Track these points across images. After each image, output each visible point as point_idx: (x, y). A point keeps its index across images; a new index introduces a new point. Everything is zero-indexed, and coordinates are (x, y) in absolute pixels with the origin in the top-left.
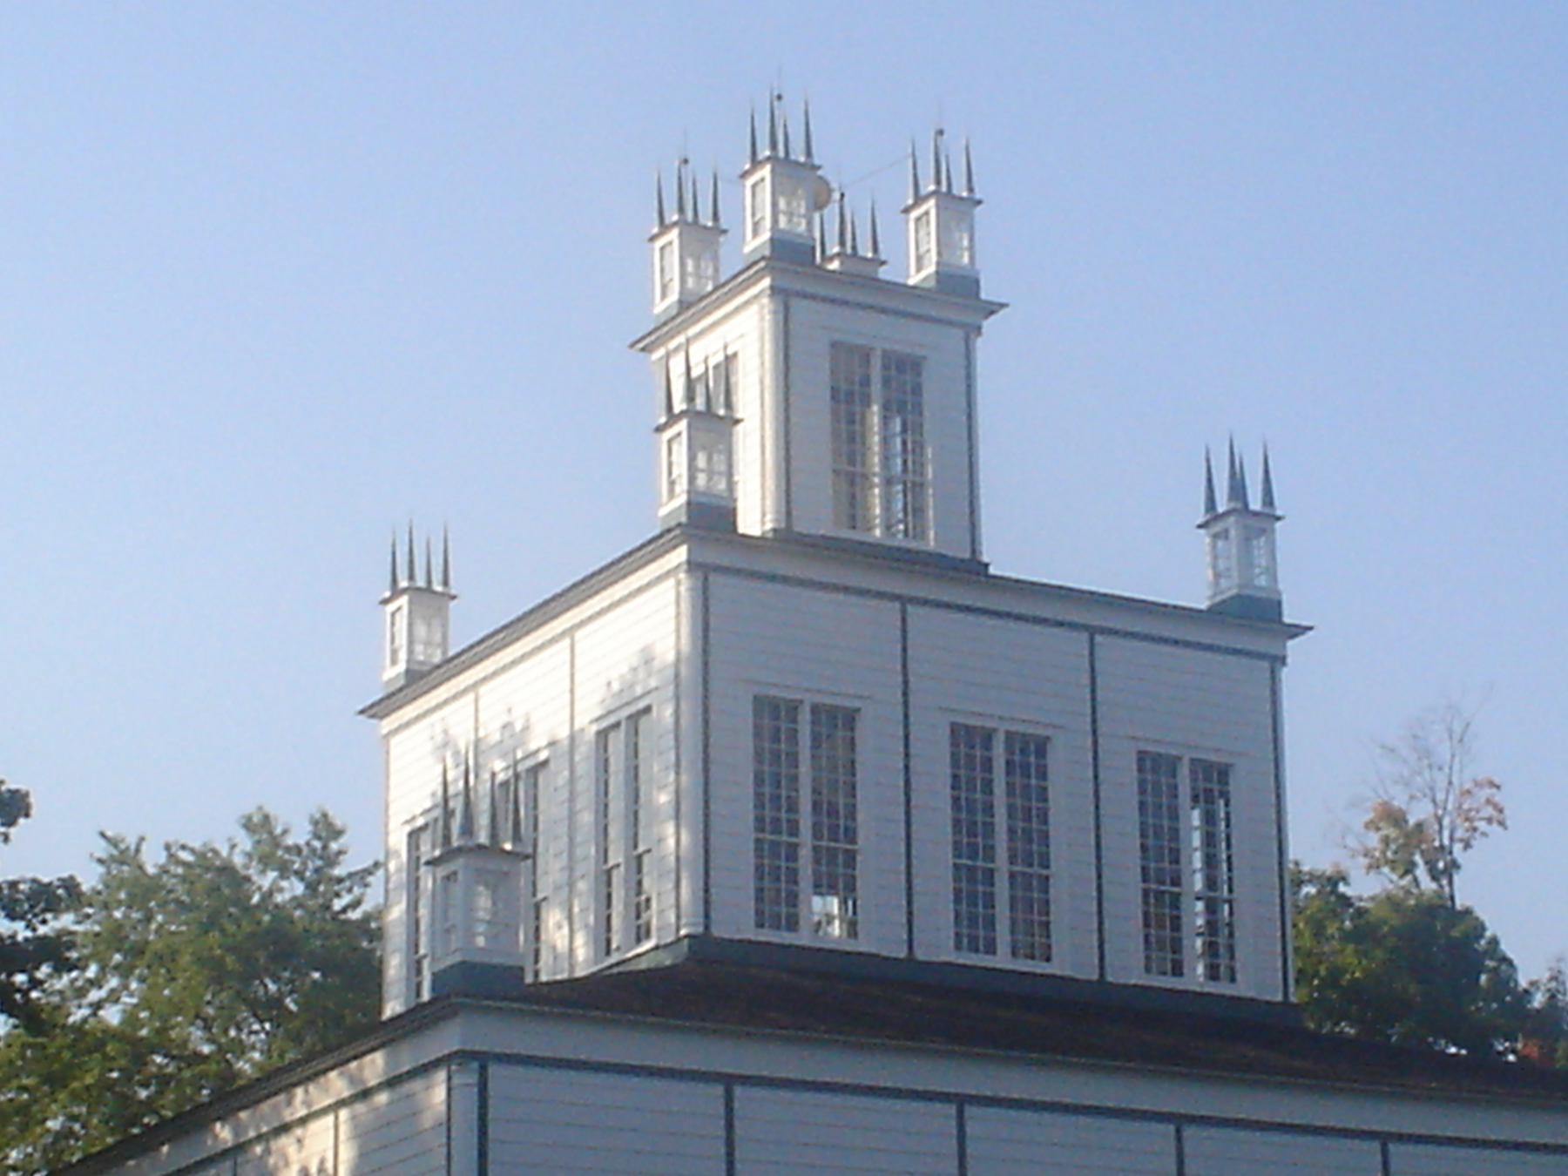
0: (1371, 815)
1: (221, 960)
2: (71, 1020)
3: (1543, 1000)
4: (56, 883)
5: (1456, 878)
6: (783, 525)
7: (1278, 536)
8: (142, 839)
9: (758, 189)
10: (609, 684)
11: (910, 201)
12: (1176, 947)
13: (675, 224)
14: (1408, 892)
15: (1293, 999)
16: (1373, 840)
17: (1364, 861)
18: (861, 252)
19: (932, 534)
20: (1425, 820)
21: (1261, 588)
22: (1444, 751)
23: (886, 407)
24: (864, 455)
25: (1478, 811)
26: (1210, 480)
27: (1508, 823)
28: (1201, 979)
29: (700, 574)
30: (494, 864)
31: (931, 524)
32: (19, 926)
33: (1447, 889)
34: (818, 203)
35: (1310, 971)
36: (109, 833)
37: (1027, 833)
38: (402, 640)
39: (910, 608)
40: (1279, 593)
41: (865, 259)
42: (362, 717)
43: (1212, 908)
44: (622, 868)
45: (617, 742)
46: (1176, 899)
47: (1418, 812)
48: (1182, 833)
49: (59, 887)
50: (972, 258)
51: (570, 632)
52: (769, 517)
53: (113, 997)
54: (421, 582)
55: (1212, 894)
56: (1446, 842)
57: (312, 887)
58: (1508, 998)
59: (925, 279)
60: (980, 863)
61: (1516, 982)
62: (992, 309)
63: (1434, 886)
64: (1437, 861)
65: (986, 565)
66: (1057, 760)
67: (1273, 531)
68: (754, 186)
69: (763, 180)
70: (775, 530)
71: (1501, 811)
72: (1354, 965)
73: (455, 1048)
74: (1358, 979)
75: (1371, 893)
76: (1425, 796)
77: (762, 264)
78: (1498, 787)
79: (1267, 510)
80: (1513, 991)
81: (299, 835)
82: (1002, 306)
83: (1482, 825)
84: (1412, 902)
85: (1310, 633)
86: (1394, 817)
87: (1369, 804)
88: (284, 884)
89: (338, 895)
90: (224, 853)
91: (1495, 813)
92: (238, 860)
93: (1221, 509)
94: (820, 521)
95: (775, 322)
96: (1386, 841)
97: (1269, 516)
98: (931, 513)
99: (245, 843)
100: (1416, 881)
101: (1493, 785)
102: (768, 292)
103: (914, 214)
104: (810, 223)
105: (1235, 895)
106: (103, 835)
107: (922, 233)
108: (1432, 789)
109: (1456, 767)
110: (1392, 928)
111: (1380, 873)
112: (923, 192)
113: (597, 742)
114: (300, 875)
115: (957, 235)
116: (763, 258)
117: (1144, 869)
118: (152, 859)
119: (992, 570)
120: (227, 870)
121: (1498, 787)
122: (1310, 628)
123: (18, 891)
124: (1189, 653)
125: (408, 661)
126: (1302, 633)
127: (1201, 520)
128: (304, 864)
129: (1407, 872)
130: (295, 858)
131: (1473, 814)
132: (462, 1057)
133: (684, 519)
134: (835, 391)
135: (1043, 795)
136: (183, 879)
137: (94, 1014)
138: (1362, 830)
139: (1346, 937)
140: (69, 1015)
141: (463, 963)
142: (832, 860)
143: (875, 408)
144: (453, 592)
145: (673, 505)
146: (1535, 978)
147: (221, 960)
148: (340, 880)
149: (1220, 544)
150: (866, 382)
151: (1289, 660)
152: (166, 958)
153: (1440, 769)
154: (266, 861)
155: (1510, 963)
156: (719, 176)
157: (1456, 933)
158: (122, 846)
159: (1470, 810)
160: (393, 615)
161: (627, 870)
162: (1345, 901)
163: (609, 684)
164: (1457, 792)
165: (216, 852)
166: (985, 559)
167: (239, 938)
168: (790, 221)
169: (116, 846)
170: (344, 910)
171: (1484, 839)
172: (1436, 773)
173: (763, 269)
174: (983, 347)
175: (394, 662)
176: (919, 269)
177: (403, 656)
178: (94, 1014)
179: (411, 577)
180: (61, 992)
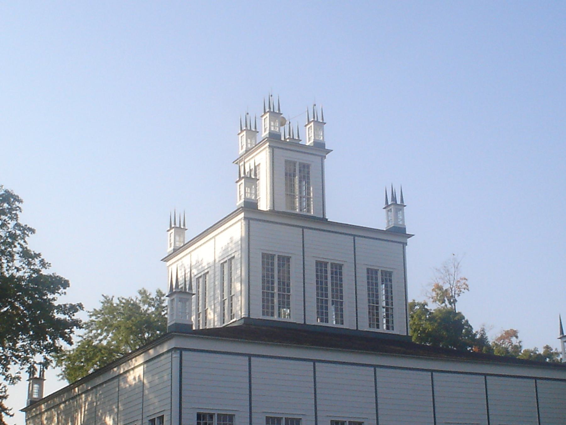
0: (434, 287)
1: (131, 328)
2: (94, 344)
3: (480, 336)
4: (77, 305)
5: (456, 304)
6: (272, 209)
7: (405, 211)
8: (113, 297)
9: (266, 120)
10: (222, 248)
11: (307, 123)
12: (378, 320)
13: (245, 130)
14: (444, 308)
15: (409, 335)
16: (434, 294)
17: (432, 300)
18: (295, 138)
19: (312, 211)
20: (448, 289)
21: (400, 225)
22: (452, 271)
23: (300, 178)
24: (294, 190)
25: (461, 286)
26: (386, 196)
27: (469, 289)
28: (385, 330)
29: (247, 220)
30: (183, 296)
31: (312, 208)
32: (67, 316)
33: (454, 307)
34: (282, 124)
35: (417, 328)
36: (105, 295)
37: (337, 290)
38: (172, 241)
39: (305, 230)
40: (405, 226)
41: (296, 139)
42: (162, 261)
43: (387, 310)
44: (227, 300)
45: (226, 266)
46: (377, 308)
47: (446, 287)
48: (379, 290)
49: (77, 306)
50: (323, 138)
51: (214, 237)
52: (268, 206)
53: (105, 338)
54: (178, 225)
55: (387, 306)
56: (453, 294)
57: (157, 309)
58: (470, 336)
59: (311, 144)
60: (324, 298)
61: (472, 332)
62: (328, 151)
63: (450, 306)
64: (451, 299)
65: (327, 219)
66: (345, 270)
67: (403, 209)
68: (265, 119)
69: (267, 117)
70: (270, 210)
71: (468, 286)
72: (429, 327)
73: (173, 347)
74: (430, 331)
75: (434, 309)
76: (447, 282)
77: (266, 139)
78: (467, 280)
79: (402, 204)
80: (471, 334)
81: (153, 295)
82: (332, 151)
83: (463, 290)
84: (445, 311)
85: (414, 236)
86: (440, 288)
87: (433, 285)
88: (150, 308)
89: (164, 311)
90: (134, 300)
91: (466, 287)
92: (138, 301)
93: (389, 203)
94: (282, 207)
95: (270, 155)
96: (437, 294)
97: (403, 205)
98: (312, 205)
99: (140, 297)
100: (446, 305)
101: (465, 279)
102: (268, 147)
103: (308, 127)
104: (279, 130)
105: (393, 307)
106: (103, 295)
107: (310, 132)
108: (449, 281)
109: (456, 275)
110: (440, 317)
111: (436, 303)
112: (310, 120)
113: (221, 266)
114: (153, 306)
115: (320, 133)
116: (267, 138)
117: (369, 300)
118: (115, 302)
119: (328, 220)
120: (134, 304)
121: (467, 280)
122: (413, 235)
123: (66, 307)
124: (383, 242)
125: (174, 247)
126: (411, 237)
127: (384, 207)
128: (154, 303)
129: (443, 303)
130: (152, 301)
131: (460, 287)
132: (175, 349)
133: (243, 206)
134: (286, 175)
135: (341, 280)
136: (123, 307)
137: (100, 342)
138: (431, 291)
139: (426, 320)
140: (93, 343)
141: (175, 323)
142: (284, 297)
143: (297, 177)
144: (186, 228)
145: (240, 202)
146: (477, 330)
147: (131, 328)
148: (164, 307)
149: (389, 213)
150: (295, 171)
151: (408, 244)
152: (118, 327)
153: (452, 275)
154: (144, 302)
155: (471, 327)
156: (256, 117)
157: (456, 318)
158: (108, 299)
159: (459, 286)
160: (170, 234)
161: (228, 300)
162: (427, 310)
163: (222, 248)
164: (456, 281)
165: (132, 300)
166: (327, 218)
167: (137, 322)
168: (274, 128)
169: (106, 299)
170: (164, 315)
171: (463, 294)
172: (451, 277)
173: (266, 141)
174: (326, 161)
175: (170, 247)
176: (309, 141)
177: (173, 245)
178: (100, 342)
179: (175, 224)
180: (91, 337)
